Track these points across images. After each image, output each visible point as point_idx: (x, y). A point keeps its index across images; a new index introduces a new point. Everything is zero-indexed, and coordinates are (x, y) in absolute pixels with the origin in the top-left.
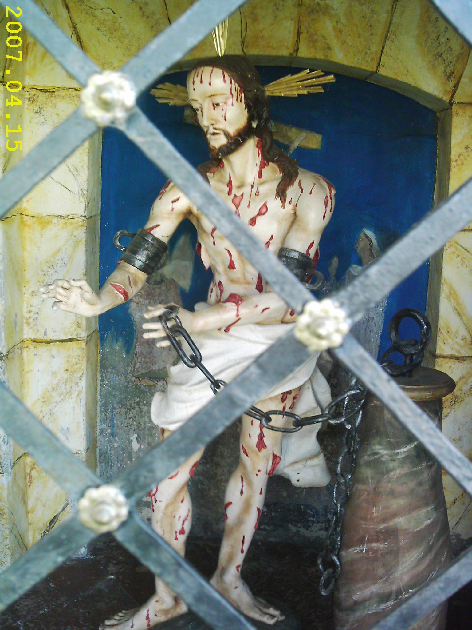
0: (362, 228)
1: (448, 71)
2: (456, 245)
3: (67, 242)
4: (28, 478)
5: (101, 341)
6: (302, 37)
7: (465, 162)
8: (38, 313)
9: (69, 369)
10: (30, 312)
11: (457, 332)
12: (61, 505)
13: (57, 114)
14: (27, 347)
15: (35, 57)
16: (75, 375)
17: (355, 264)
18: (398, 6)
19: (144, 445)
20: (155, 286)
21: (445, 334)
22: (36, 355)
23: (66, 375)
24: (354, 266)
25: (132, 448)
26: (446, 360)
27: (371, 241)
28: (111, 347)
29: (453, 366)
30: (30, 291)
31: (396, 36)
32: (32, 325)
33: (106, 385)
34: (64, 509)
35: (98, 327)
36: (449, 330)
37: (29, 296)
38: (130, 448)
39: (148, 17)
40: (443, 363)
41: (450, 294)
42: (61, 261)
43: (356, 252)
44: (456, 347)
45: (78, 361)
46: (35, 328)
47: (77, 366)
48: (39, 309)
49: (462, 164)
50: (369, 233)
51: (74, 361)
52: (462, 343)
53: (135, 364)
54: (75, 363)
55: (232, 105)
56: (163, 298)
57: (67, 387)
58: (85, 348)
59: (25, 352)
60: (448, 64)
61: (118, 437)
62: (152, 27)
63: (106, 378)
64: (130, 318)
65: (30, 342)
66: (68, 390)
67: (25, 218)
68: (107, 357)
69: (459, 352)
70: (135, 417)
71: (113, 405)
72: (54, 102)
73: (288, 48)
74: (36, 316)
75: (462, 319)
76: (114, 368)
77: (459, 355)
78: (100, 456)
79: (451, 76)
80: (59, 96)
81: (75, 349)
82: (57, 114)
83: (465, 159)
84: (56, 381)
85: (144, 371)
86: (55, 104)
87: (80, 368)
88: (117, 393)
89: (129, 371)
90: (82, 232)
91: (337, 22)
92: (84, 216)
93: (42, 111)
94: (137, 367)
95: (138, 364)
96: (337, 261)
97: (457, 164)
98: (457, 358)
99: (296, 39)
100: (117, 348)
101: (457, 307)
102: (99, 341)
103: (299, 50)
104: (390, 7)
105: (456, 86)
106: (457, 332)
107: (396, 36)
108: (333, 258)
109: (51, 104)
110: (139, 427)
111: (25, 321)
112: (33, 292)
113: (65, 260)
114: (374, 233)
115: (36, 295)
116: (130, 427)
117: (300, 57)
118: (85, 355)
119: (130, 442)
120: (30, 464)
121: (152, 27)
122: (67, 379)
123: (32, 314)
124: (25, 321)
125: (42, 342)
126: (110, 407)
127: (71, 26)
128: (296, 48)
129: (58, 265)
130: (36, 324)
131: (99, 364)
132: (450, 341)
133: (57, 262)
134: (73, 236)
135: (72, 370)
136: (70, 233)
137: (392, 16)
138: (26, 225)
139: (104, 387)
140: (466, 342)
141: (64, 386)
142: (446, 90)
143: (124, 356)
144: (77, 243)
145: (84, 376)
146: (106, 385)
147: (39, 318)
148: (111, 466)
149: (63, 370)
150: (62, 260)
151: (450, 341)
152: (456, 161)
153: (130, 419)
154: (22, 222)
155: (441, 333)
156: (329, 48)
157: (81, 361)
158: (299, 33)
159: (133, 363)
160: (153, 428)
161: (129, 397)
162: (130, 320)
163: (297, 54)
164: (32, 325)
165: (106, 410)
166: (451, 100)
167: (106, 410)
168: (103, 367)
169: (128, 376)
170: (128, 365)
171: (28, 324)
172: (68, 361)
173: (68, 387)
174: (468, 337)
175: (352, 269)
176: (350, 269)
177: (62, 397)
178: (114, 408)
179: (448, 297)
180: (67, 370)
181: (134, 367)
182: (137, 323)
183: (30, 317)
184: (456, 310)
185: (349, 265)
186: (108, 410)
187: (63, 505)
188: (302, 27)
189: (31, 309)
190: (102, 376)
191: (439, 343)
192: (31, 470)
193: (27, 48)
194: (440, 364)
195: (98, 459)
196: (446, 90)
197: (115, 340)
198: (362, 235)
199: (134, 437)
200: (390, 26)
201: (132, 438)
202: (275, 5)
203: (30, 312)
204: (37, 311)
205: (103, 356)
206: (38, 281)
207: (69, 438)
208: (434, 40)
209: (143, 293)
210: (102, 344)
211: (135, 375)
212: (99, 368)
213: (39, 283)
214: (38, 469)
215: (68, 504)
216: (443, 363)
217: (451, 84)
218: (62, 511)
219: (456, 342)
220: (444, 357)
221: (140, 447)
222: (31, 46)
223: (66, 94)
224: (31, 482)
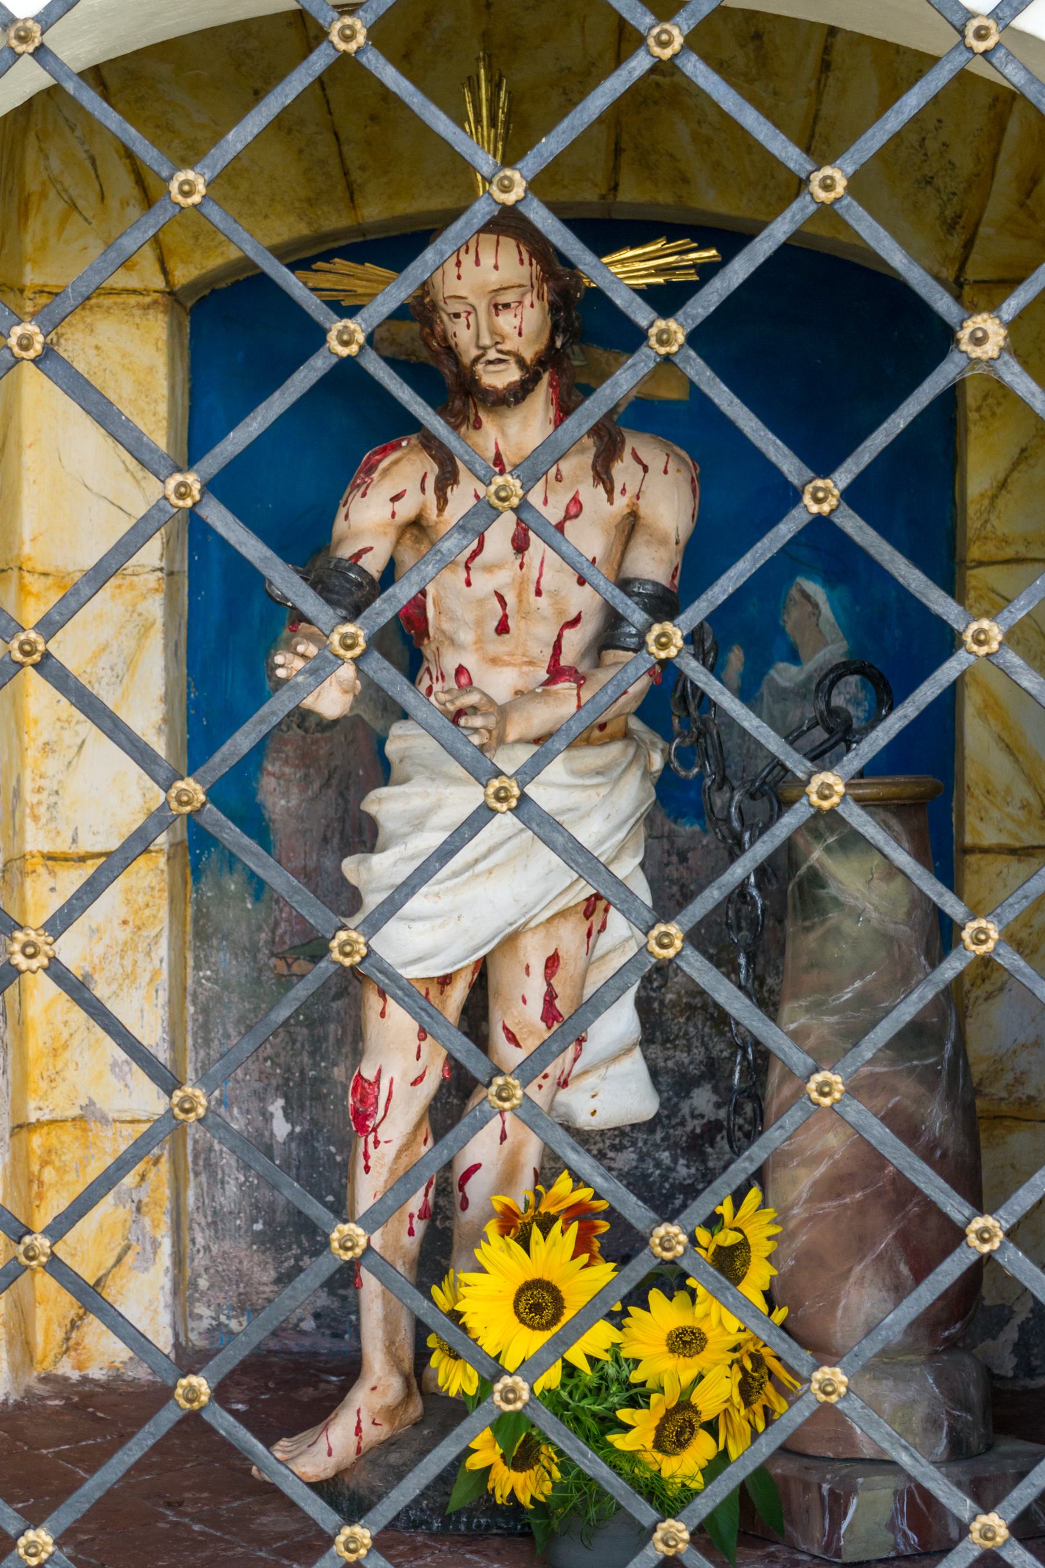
0: (792, 578)
1: (949, 213)
2: (993, 595)
3: (122, 627)
4: (35, 1187)
5: (193, 872)
6: (625, 158)
7: (999, 411)
8: (57, 792)
9: (130, 919)
10: (40, 790)
11: (1008, 791)
12: (112, 1250)
13: (97, 347)
14: (34, 871)
15: (45, 223)
16: (144, 933)
17: (782, 660)
18: (831, 81)
19: (302, 1124)
20: (319, 735)
21: (982, 798)
22: (53, 890)
23: (122, 935)
24: (781, 665)
25: (272, 1134)
26: (990, 857)
27: (816, 606)
28: (219, 887)
29: (1005, 870)
30: (40, 742)
31: (829, 145)
32: (43, 820)
33: (208, 979)
34: (119, 1260)
35: (186, 836)
36: (990, 788)
37: (38, 755)
38: (267, 1133)
39: (289, 131)
40: (982, 863)
41: (986, 707)
42: (109, 672)
43: (782, 631)
44: (1009, 825)
45: (150, 899)
46: (52, 826)
47: (147, 912)
48: (60, 782)
49: (993, 414)
50: (814, 589)
51: (141, 900)
52: (1021, 815)
53: (277, 924)
54: (142, 905)
55: (532, 306)
56: (338, 763)
57: (125, 962)
58: (165, 868)
59: (29, 882)
60: (949, 200)
61: (240, 1108)
62: (301, 151)
63: (207, 962)
64: (262, 815)
65: (39, 860)
66: (129, 969)
67: (28, 578)
68: (208, 912)
69: (1017, 838)
70: (278, 1055)
71: (225, 1029)
72: (88, 321)
73: (596, 185)
74: (53, 799)
75: (1017, 760)
76: (225, 937)
77: (1017, 845)
78: (196, 1157)
79: (956, 223)
80: (99, 306)
81: (142, 873)
82: (97, 347)
83: (999, 404)
84: (99, 949)
85: (297, 941)
86: (91, 325)
87: (155, 917)
88: (235, 998)
89: (261, 943)
90: (157, 605)
91: (699, 122)
92: (161, 569)
93: (62, 341)
94: (280, 931)
95: (283, 925)
96: (742, 655)
97: (982, 417)
98: (1012, 851)
99: (611, 164)
100: (233, 887)
101: (1005, 735)
102: (188, 871)
103: (621, 188)
104: (812, 85)
105: (968, 245)
106: (1008, 791)
107: (829, 145)
108: (731, 650)
109: (81, 326)
110: (287, 1080)
111: (28, 811)
112: (48, 744)
113: (120, 668)
114: (824, 586)
115: (53, 751)
116: (266, 1081)
117: (621, 203)
118: (165, 886)
119: (268, 1118)
120: (39, 1152)
121: (301, 151)
122: (125, 943)
123: (44, 795)
124: (28, 811)
125: (66, 860)
126: (217, 1033)
127: (123, 153)
128: (613, 184)
129: (104, 682)
130: (52, 819)
131: (189, 928)
132: (995, 813)
133: (101, 673)
134: (135, 615)
135: (138, 923)
136: (130, 609)
137: (819, 101)
138: (30, 593)
139: (202, 985)
140: (1030, 812)
141: (118, 960)
142: (947, 256)
143: (249, 906)
144: (146, 629)
145: (165, 934)
146: (208, 979)
147: (59, 803)
148: (222, 1182)
149: (116, 922)
150: (112, 669)
151: (995, 813)
152: (978, 409)
153: (265, 1060)
154: (22, 587)
155: (972, 796)
156: (685, 180)
157: (158, 901)
158: (618, 151)
159: (271, 921)
160: (323, 1081)
161: (263, 1006)
162: (261, 817)
163: (615, 196)
164: (43, 820)
165: (207, 1042)
166: (958, 278)
167: (207, 1042)
168: (201, 935)
169: (260, 956)
170: (260, 929)
171: (36, 818)
172: (128, 902)
173: (128, 962)
174: (1034, 801)
175: (777, 672)
176: (772, 672)
177: (114, 986)
178: (228, 1036)
179: (981, 714)
180: (125, 922)
181: (273, 932)
182: (277, 825)
183: (39, 803)
184: (1003, 740)
185: (769, 664)
186: (212, 1040)
187: (118, 1250)
188: (625, 137)
189: (42, 782)
190: (197, 958)
191: (971, 820)
192: (42, 1167)
193: (26, 205)
194: (975, 867)
195: (190, 1165)
196: (947, 256)
197: (226, 869)
198: (794, 592)
199: (277, 1107)
200: (815, 123)
201: (271, 1108)
202: (565, 93)
203: (40, 790)
204: (55, 788)
205: (199, 910)
206: (59, 719)
207: (131, 1084)
208: (913, 147)
209: (291, 754)
210: (197, 879)
211: (275, 951)
212: (189, 937)
213: (58, 724)
214: (57, 1163)
215: (128, 1248)
216: (982, 863)
217: (956, 242)
218: (115, 1265)
219: (1009, 815)
220: (985, 851)
221: (293, 1130)
222: (34, 199)
223: (116, 303)
224: (40, 1196)
